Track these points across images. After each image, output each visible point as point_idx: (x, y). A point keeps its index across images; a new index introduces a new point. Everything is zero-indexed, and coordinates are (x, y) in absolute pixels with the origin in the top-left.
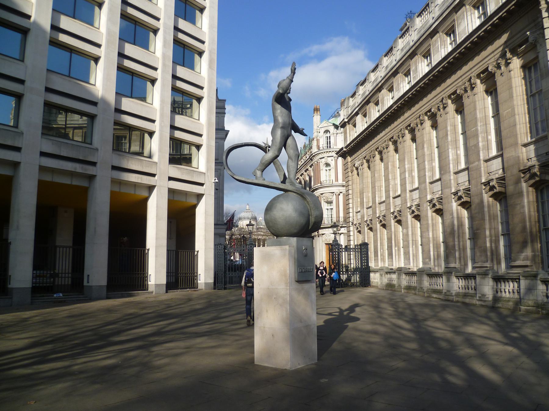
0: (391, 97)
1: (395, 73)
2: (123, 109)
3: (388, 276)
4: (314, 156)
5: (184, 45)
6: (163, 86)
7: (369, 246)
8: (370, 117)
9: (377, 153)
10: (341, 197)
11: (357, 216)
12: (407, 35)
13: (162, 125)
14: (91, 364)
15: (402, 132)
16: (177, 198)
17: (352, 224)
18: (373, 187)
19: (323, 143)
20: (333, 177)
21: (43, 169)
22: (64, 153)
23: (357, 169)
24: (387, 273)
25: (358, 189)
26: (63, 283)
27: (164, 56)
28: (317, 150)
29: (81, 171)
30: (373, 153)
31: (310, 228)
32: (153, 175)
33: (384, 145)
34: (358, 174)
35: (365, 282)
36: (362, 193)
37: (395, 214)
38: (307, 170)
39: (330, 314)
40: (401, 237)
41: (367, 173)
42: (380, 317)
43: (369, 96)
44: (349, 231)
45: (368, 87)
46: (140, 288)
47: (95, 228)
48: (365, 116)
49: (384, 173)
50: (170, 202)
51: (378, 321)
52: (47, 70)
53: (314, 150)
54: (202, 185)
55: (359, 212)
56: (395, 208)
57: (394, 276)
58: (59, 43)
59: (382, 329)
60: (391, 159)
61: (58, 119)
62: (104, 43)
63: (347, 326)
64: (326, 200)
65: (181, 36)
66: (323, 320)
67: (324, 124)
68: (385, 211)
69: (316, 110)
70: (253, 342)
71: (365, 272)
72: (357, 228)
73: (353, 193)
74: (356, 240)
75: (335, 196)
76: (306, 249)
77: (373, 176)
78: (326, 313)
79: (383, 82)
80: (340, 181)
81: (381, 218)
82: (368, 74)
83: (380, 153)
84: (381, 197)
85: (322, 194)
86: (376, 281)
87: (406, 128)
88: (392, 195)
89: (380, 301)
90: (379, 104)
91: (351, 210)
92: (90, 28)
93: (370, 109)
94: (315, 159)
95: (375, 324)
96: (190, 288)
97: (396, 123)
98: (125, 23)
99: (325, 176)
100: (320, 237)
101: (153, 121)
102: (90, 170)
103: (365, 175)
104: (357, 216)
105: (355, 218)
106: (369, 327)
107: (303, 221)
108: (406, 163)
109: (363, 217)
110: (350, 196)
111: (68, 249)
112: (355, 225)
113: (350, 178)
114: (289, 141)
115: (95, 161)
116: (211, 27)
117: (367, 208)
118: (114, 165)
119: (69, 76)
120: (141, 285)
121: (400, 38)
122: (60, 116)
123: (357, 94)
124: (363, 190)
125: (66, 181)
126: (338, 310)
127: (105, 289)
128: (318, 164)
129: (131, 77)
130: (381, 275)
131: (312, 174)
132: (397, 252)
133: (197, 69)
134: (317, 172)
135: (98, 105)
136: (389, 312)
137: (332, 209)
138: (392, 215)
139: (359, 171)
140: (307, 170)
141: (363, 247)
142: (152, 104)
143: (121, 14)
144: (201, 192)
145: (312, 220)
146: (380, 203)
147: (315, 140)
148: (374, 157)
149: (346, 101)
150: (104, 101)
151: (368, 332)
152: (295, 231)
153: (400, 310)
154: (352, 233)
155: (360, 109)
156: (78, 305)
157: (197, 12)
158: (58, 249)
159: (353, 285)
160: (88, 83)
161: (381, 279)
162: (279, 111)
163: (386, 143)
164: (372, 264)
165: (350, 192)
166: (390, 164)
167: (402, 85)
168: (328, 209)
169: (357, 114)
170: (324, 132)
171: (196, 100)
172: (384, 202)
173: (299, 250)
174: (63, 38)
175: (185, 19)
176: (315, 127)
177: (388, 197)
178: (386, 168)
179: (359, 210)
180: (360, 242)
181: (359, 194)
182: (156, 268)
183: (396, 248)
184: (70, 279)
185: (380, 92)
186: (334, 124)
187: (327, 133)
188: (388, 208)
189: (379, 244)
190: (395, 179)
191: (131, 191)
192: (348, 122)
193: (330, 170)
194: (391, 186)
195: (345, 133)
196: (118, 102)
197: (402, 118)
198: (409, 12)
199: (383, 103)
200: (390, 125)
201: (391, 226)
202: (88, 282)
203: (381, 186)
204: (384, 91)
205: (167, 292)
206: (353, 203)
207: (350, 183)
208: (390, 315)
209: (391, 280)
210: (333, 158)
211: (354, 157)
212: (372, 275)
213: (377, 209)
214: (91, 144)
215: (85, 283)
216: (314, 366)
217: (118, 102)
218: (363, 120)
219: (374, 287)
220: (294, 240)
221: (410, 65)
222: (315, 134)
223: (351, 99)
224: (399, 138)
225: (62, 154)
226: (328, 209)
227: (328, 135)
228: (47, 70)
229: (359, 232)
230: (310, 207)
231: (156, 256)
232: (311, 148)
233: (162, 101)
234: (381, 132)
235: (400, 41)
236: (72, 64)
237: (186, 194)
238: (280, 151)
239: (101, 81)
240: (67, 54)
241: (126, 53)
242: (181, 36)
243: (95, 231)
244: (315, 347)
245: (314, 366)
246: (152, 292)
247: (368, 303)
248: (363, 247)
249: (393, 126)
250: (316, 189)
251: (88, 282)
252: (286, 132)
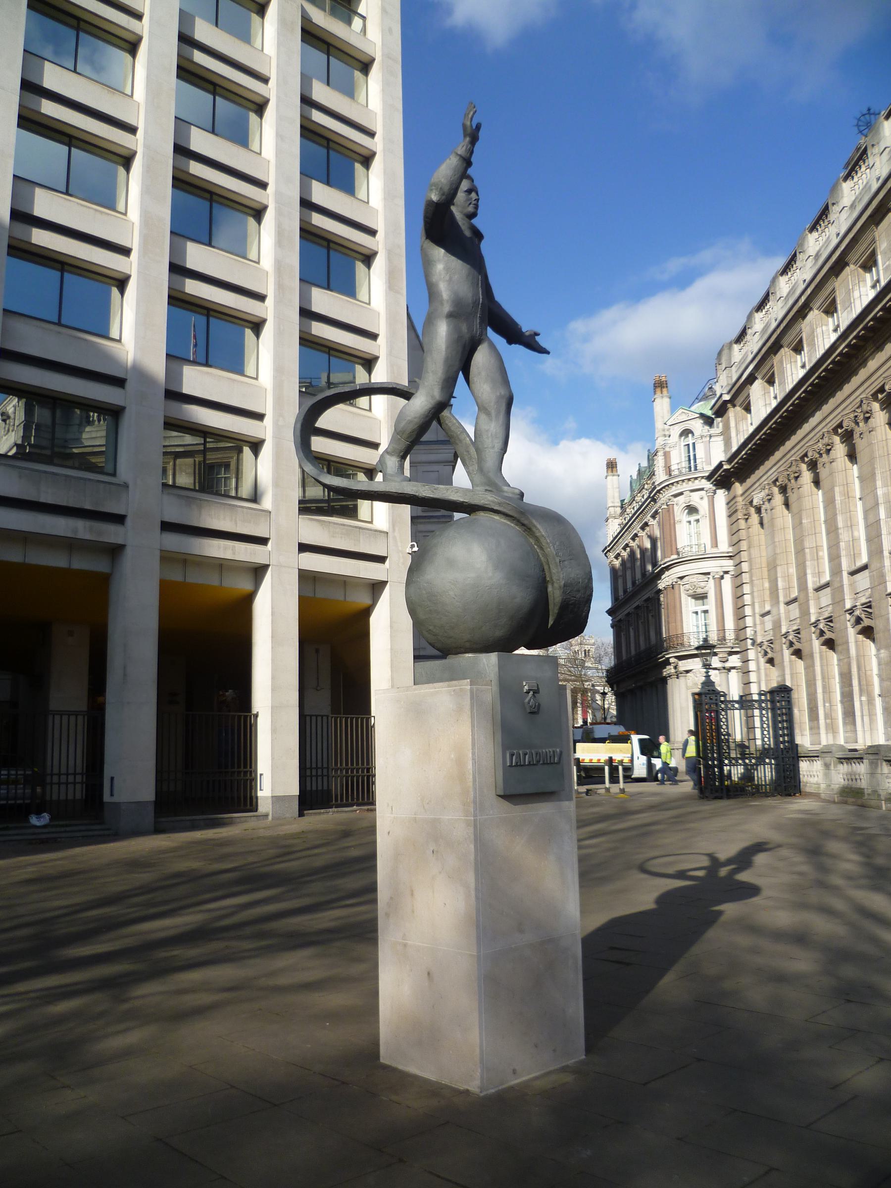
0: (831, 327)
1: (837, 267)
2: (186, 390)
3: (844, 768)
4: (659, 491)
5: (329, 241)
6: (279, 333)
7: (794, 695)
8: (783, 383)
9: (804, 467)
10: (727, 584)
11: (763, 623)
12: (863, 168)
13: (280, 423)
15: (865, 407)
16: (322, 593)
17: (753, 644)
18: (800, 552)
19: (678, 459)
20: (706, 539)
22: (47, 497)
23: (758, 510)
24: (841, 760)
25: (764, 560)
26: (314, 788)
27: (279, 266)
28: (666, 477)
29: (88, 537)
30: (794, 468)
31: (551, 622)
32: (263, 541)
33: (820, 445)
34: (761, 524)
35: (788, 783)
36: (772, 567)
37: (857, 613)
38: (646, 524)
39: (681, 875)
40: (875, 671)
41: (784, 518)
42: (822, 885)
43: (778, 331)
44: (746, 661)
45: (777, 310)
46: (245, 805)
47: (125, 668)
48: (771, 381)
49: (826, 512)
50: (304, 602)
51: (815, 896)
52: (4, 310)
53: (660, 476)
54: (381, 559)
55: (768, 613)
56: (856, 599)
57: (862, 768)
59: (821, 925)
60: (839, 478)
61: (84, 436)
62: (135, 244)
63: (720, 913)
64: (691, 592)
65: (318, 220)
66: (655, 895)
67: (680, 415)
68: (830, 609)
69: (660, 385)
71: (787, 757)
72: (766, 653)
73: (751, 569)
74: (763, 679)
75: (711, 581)
76: (536, 692)
77: (798, 525)
78: (671, 871)
79: (809, 291)
80: (724, 546)
81: (821, 626)
82: (774, 281)
83: (813, 466)
84: (819, 574)
85: (681, 578)
86: (813, 780)
87: (875, 396)
88: (846, 565)
89: (827, 834)
90: (802, 349)
91: (748, 611)
92: (101, 212)
93: (781, 362)
94: (663, 498)
95: (804, 906)
96: (358, 805)
97: (847, 388)
98: (191, 200)
99: (688, 535)
100: (682, 679)
101: (260, 417)
102: (111, 534)
103: (779, 522)
104: (763, 623)
105: (758, 628)
106: (784, 919)
107: (520, 597)
108: (879, 483)
109: (777, 625)
110: (745, 578)
111: (73, 718)
112: (761, 645)
113: (743, 534)
114: (481, 358)
115: (122, 512)
116: (388, 196)
117: (788, 603)
118: (167, 519)
119: (59, 324)
120: (239, 798)
121: (845, 179)
122: (88, 429)
123: (749, 332)
124: (775, 560)
125: (57, 560)
126: (705, 862)
127: (151, 808)
128: (670, 509)
129: (205, 318)
130: (827, 766)
131: (657, 533)
132: (866, 708)
133: (362, 294)
134: (668, 526)
135: (128, 385)
136: (848, 866)
137: (706, 612)
138: (848, 617)
139: (764, 514)
140: (646, 524)
141: (780, 698)
142: (256, 379)
143: (174, 178)
144: (382, 577)
145: (555, 594)
146: (818, 589)
147: (660, 454)
148: (796, 478)
149: (725, 352)
150: (139, 371)
151: (779, 935)
152: (499, 633)
153: (880, 861)
154: (752, 666)
155: (757, 368)
156: (77, 850)
157: (358, 166)
158: (51, 717)
159: (758, 792)
160: (107, 337)
161: (827, 775)
162: (440, 267)
163: (826, 440)
164: (804, 740)
165: (745, 567)
166: (837, 489)
167: (856, 294)
168: (697, 613)
169: (751, 379)
170: (681, 435)
171: (363, 365)
172: (827, 585)
173: (507, 689)
174: (41, 238)
175: (328, 182)
176: (659, 425)
177: (836, 571)
178: (830, 502)
179: (767, 608)
180: (774, 684)
181: (765, 570)
182: (273, 759)
183: (864, 698)
184: (78, 787)
185: (804, 317)
186: (702, 416)
187: (687, 436)
188: (838, 600)
189: (820, 690)
190: (851, 526)
191: (211, 579)
192: (732, 401)
193: (698, 521)
194: (842, 545)
195: (727, 427)
196: (173, 374)
197: (863, 374)
198: (865, 111)
199: (812, 344)
200: (832, 394)
201: (847, 643)
202: (112, 795)
203: (818, 548)
204: (814, 315)
205: (301, 815)
206: (752, 593)
207: (744, 545)
208: (849, 877)
209: (852, 777)
210: (703, 493)
211: (749, 482)
212: (804, 765)
213: (812, 603)
214: (114, 474)
215: (107, 798)
216: (568, 1078)
217: (173, 374)
218: (766, 393)
219: (809, 795)
220: (490, 661)
221: (874, 241)
222: (660, 441)
223: (736, 347)
224: (857, 424)
225: (42, 500)
226: (697, 613)
227: (690, 440)
228: (4, 310)
229: (771, 661)
230: (545, 556)
231: (274, 731)
232: (653, 474)
233: (279, 370)
234: (812, 415)
235: (846, 186)
236: (64, 293)
237: (343, 582)
238: (449, 385)
239: (136, 331)
240: (53, 275)
241: (190, 264)
242: (318, 220)
243: (125, 675)
244: (576, 1009)
245: (568, 1078)
246: (266, 816)
247: (794, 840)
248: (780, 698)
249: (840, 396)
250: (668, 568)
251: (112, 795)
252: (464, 328)
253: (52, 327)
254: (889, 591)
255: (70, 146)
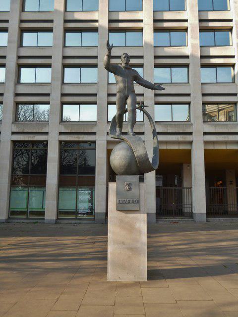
14: (53, 249)
21: (206, 142)
29: (182, 140)
58: (210, 28)
70: (107, 257)
102: (188, 138)
118: (13, 131)
119: (217, 83)
125: (176, 147)
127: (155, 216)
152: (123, 171)
225: (169, 132)
253: (169, 84)
254: (3, 70)
255: (214, 32)
